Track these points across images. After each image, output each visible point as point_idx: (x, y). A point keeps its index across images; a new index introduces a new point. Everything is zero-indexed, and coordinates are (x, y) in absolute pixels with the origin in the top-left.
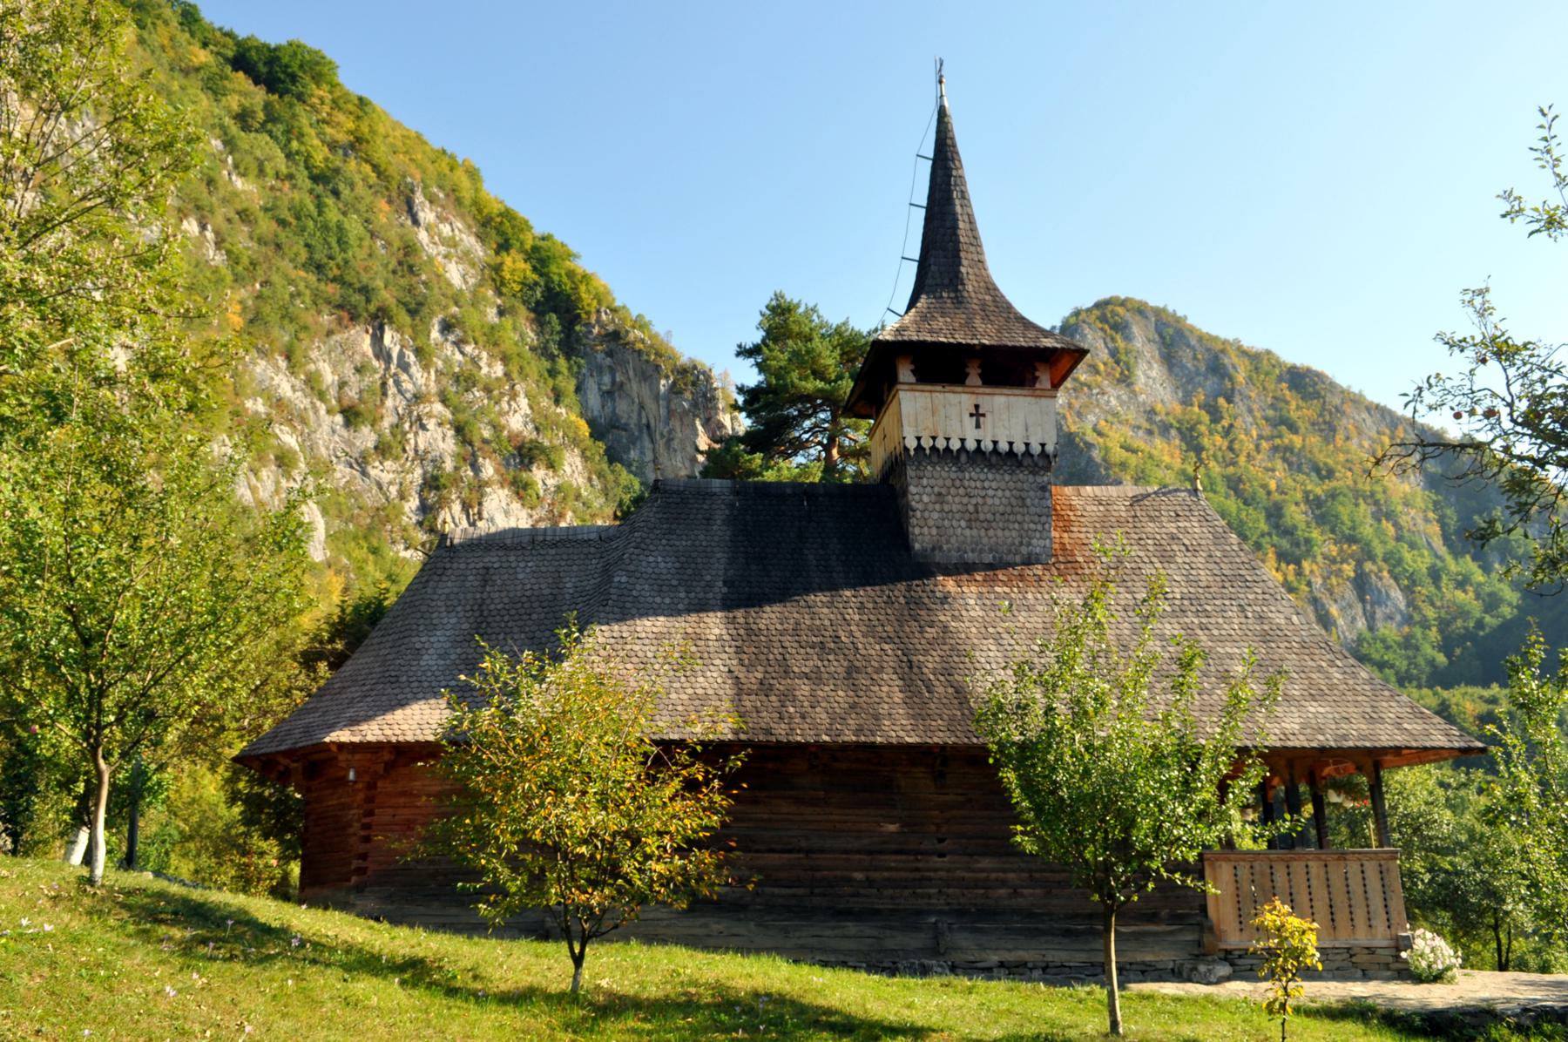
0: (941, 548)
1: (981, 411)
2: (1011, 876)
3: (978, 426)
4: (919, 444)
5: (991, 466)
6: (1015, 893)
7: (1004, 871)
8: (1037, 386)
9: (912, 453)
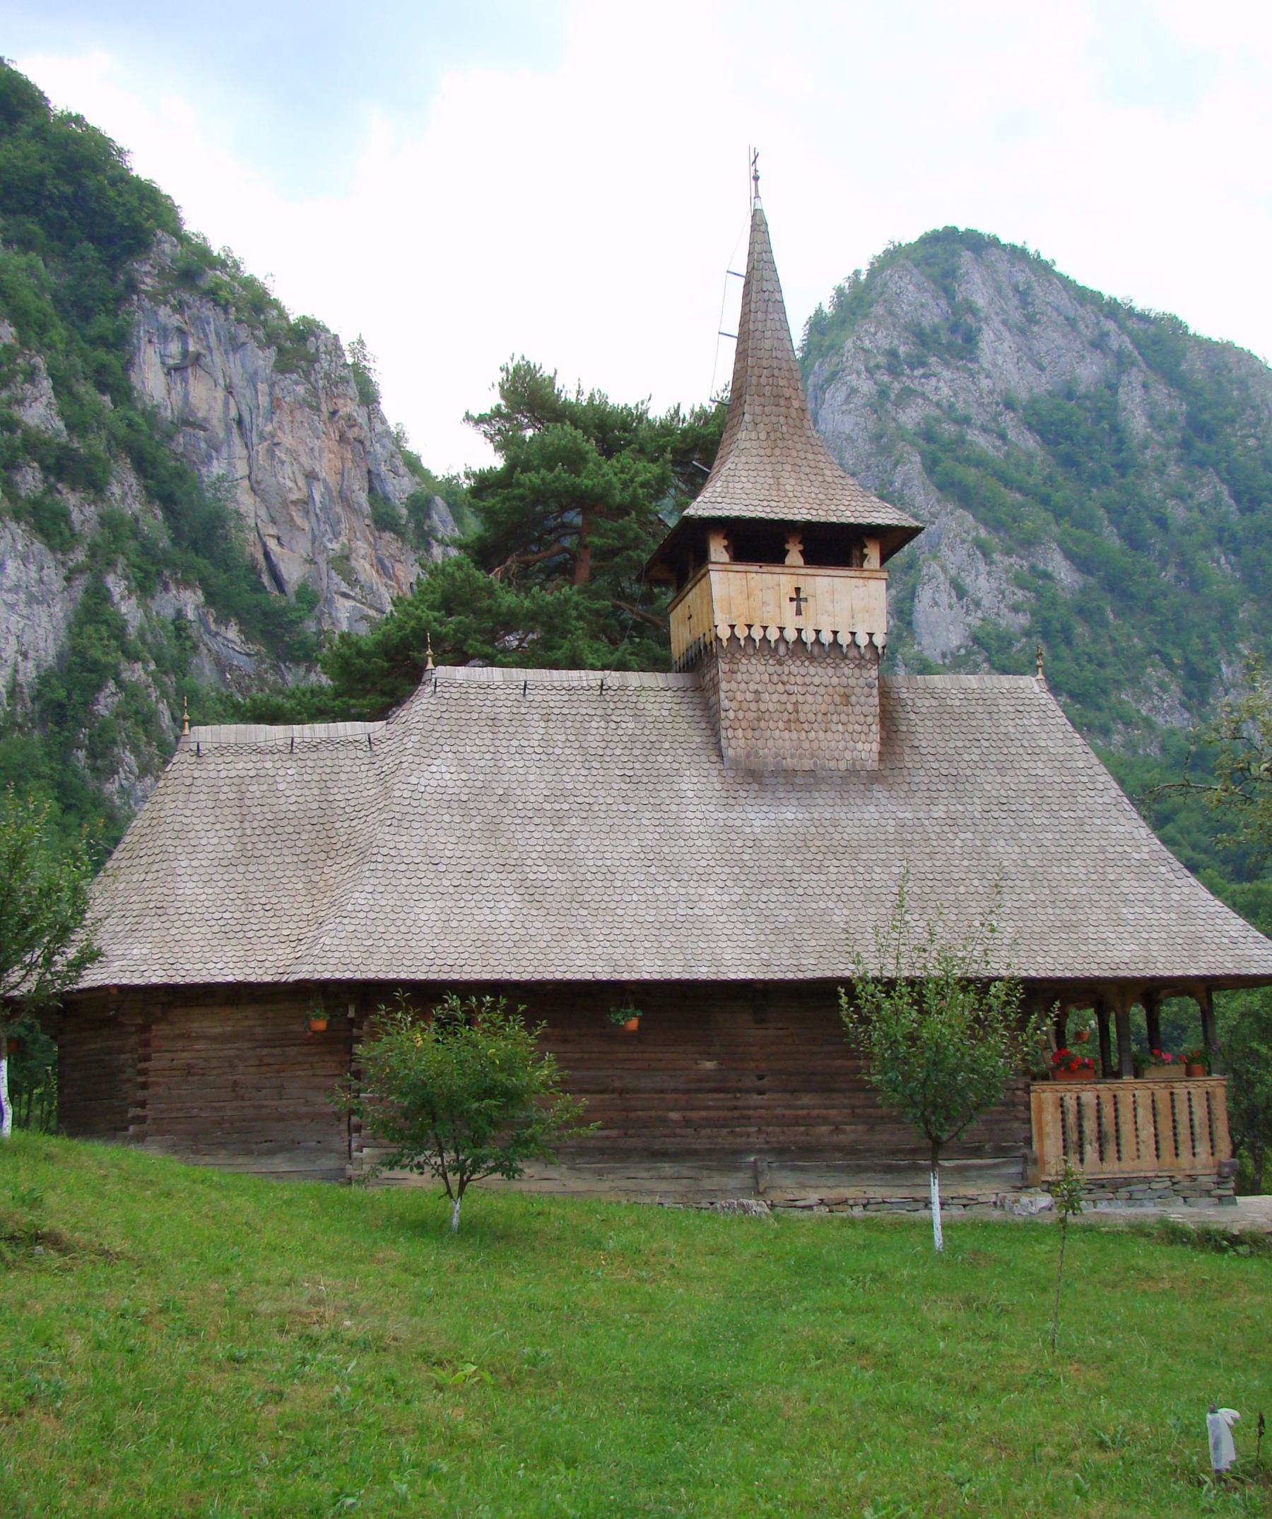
1: (802, 596)
2: (833, 1112)
3: (799, 612)
4: (733, 633)
5: (812, 659)
6: (837, 1130)
7: (827, 1108)
9: (725, 643)
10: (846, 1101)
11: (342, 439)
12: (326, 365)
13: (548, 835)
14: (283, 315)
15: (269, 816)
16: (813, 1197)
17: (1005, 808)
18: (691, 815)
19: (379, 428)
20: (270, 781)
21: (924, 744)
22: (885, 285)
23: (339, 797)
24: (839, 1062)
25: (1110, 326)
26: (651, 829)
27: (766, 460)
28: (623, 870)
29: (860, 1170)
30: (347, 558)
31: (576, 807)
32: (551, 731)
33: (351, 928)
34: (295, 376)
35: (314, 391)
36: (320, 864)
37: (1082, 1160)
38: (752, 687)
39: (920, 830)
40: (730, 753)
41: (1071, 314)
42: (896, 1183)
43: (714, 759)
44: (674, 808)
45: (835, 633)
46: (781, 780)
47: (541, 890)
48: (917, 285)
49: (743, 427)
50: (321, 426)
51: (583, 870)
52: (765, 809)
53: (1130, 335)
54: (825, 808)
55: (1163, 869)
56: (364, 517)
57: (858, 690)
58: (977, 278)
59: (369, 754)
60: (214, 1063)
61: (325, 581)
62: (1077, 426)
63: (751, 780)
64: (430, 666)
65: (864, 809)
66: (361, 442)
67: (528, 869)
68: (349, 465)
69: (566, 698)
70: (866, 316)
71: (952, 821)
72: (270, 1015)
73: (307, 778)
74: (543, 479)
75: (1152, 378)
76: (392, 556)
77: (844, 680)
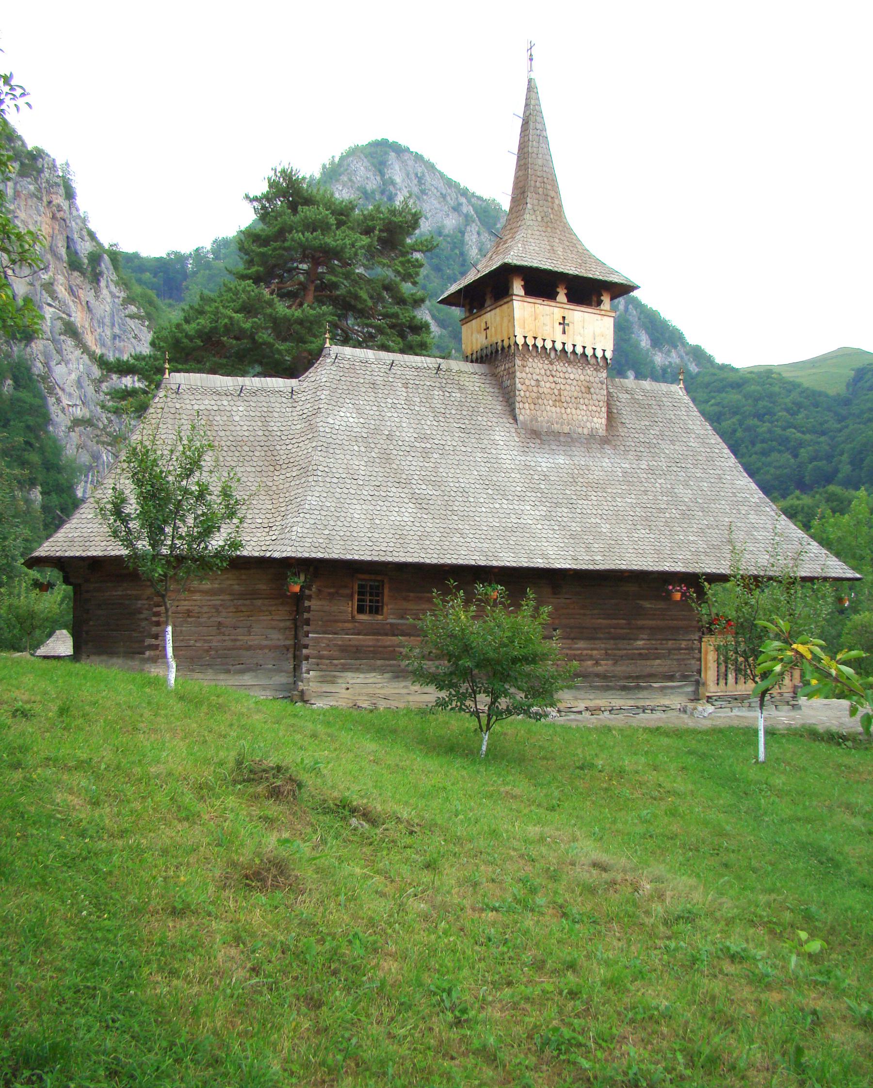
0: (537, 419)
1: (566, 322)
2: (595, 652)
3: (564, 332)
4: (525, 342)
5: (569, 362)
6: (597, 663)
7: (592, 649)
8: (602, 307)
9: (520, 348)
10: (603, 646)
11: (54, 217)
12: (47, 175)
13: (421, 464)
14: (24, 144)
15: (231, 438)
16: (581, 706)
17: (679, 465)
18: (505, 457)
19: (75, 213)
20: (228, 414)
21: (627, 421)
22: (349, 165)
23: (275, 428)
24: (600, 621)
25: (463, 200)
26: (482, 464)
27: (543, 234)
28: (473, 491)
29: (608, 688)
30: (52, 284)
31: (435, 446)
32: (411, 395)
33: (312, 522)
34: (29, 180)
35: (39, 189)
36: (270, 474)
37: (726, 684)
38: (535, 377)
39: (635, 475)
40: (521, 418)
41: (444, 192)
42: (629, 697)
43: (512, 421)
44: (494, 452)
45: (584, 347)
46: (552, 438)
47: (426, 501)
48: (366, 168)
49: (527, 211)
50: (42, 209)
51: (448, 489)
52: (546, 455)
53: (473, 206)
54: (580, 458)
55: (768, 509)
56: (63, 262)
57: (595, 385)
58: (397, 167)
59: (290, 401)
60: (205, 609)
61: (39, 295)
62: (443, 250)
63: (534, 436)
64: (327, 345)
65: (602, 459)
66: (64, 220)
67: (414, 487)
68: (56, 232)
69: (416, 374)
70: (337, 181)
71: (651, 470)
72: (244, 577)
73: (252, 414)
74: (307, 239)
75: (482, 230)
76: (78, 285)
77: (587, 378)
